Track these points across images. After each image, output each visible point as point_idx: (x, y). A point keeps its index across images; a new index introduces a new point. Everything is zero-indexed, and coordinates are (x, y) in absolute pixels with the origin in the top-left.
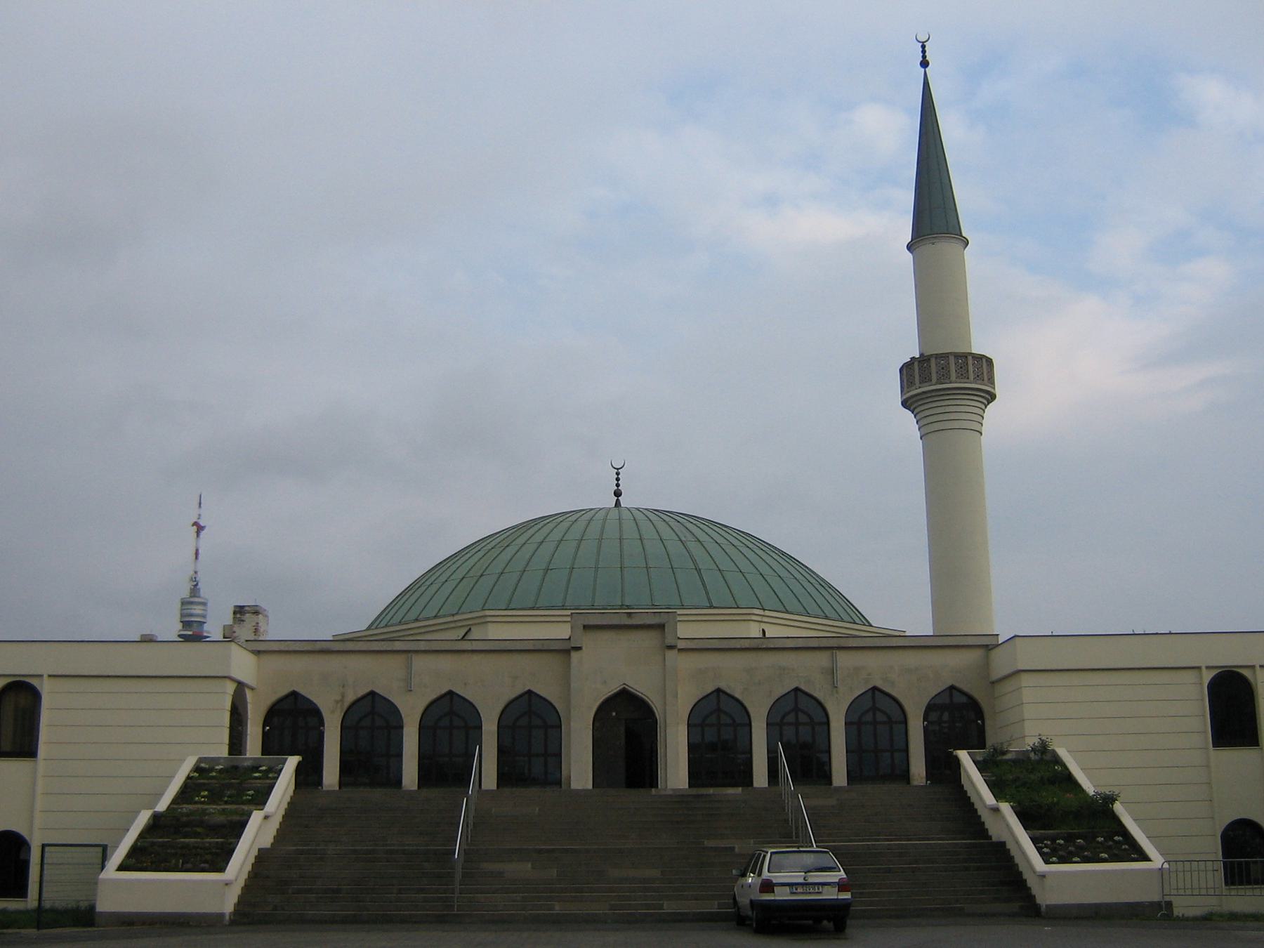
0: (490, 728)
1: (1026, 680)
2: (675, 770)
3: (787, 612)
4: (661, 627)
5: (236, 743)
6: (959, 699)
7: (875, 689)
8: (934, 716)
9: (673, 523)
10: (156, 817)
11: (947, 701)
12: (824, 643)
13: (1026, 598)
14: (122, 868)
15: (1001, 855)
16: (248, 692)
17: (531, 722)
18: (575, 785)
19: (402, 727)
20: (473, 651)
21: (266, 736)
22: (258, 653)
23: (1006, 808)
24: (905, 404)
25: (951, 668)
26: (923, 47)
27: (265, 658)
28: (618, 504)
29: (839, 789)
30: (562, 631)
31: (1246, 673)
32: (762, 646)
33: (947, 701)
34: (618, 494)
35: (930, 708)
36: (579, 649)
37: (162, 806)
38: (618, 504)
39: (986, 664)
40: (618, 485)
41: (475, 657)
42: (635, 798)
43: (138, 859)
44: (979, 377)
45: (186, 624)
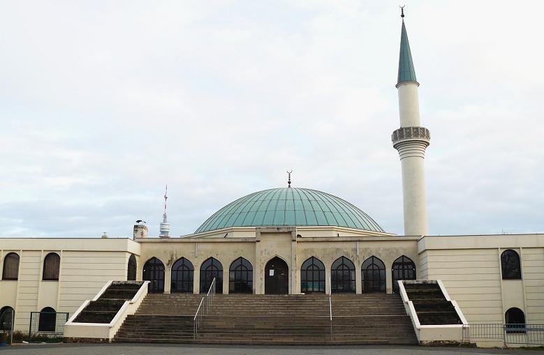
0: (226, 271)
1: (428, 253)
2: (295, 287)
4: (290, 233)
5: (132, 274)
6: (406, 260)
7: (373, 256)
8: (396, 267)
9: (307, 194)
10: (92, 303)
12: (353, 239)
13: (437, 222)
14: (74, 321)
15: (408, 319)
16: (136, 257)
17: (242, 269)
18: (257, 293)
19: (193, 271)
20: (149, 242)
21: (144, 274)
22: (141, 243)
23: (411, 303)
25: (405, 249)
27: (144, 245)
28: (289, 186)
30: (253, 235)
32: (328, 241)
35: (394, 264)
37: (95, 299)
38: (289, 186)
39: (417, 248)
41: (221, 245)
42: (245, 297)
43: (83, 317)
44: (423, 136)
45: (162, 232)
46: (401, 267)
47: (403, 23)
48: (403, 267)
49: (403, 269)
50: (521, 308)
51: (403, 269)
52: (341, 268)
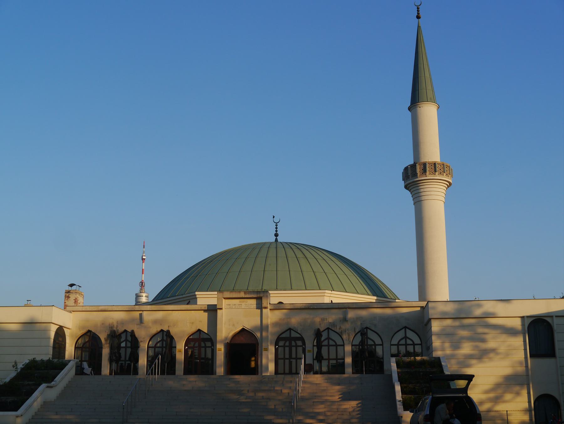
0: (144, 346)
3: (346, 292)
6: (294, 335)
11: (289, 336)
24: (406, 187)
26: (418, 8)
28: (276, 240)
29: (105, 376)
31: (548, 319)
33: (289, 336)
34: (276, 235)
36: (221, 309)
38: (276, 240)
40: (276, 231)
46: (287, 344)
47: (419, 27)
48: (290, 343)
49: (290, 347)
50: (555, 394)
51: (290, 347)
52: (403, 342)
